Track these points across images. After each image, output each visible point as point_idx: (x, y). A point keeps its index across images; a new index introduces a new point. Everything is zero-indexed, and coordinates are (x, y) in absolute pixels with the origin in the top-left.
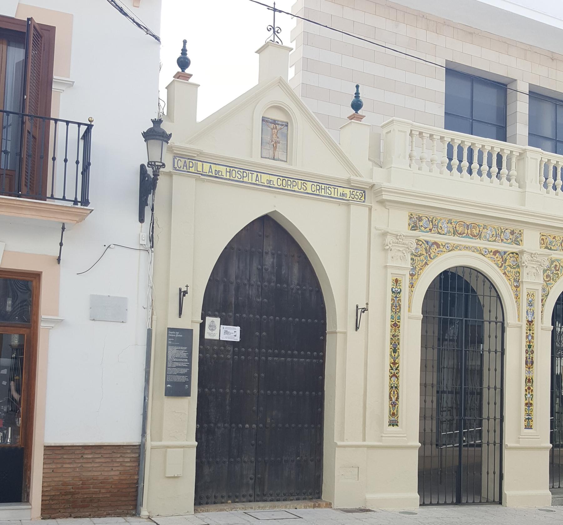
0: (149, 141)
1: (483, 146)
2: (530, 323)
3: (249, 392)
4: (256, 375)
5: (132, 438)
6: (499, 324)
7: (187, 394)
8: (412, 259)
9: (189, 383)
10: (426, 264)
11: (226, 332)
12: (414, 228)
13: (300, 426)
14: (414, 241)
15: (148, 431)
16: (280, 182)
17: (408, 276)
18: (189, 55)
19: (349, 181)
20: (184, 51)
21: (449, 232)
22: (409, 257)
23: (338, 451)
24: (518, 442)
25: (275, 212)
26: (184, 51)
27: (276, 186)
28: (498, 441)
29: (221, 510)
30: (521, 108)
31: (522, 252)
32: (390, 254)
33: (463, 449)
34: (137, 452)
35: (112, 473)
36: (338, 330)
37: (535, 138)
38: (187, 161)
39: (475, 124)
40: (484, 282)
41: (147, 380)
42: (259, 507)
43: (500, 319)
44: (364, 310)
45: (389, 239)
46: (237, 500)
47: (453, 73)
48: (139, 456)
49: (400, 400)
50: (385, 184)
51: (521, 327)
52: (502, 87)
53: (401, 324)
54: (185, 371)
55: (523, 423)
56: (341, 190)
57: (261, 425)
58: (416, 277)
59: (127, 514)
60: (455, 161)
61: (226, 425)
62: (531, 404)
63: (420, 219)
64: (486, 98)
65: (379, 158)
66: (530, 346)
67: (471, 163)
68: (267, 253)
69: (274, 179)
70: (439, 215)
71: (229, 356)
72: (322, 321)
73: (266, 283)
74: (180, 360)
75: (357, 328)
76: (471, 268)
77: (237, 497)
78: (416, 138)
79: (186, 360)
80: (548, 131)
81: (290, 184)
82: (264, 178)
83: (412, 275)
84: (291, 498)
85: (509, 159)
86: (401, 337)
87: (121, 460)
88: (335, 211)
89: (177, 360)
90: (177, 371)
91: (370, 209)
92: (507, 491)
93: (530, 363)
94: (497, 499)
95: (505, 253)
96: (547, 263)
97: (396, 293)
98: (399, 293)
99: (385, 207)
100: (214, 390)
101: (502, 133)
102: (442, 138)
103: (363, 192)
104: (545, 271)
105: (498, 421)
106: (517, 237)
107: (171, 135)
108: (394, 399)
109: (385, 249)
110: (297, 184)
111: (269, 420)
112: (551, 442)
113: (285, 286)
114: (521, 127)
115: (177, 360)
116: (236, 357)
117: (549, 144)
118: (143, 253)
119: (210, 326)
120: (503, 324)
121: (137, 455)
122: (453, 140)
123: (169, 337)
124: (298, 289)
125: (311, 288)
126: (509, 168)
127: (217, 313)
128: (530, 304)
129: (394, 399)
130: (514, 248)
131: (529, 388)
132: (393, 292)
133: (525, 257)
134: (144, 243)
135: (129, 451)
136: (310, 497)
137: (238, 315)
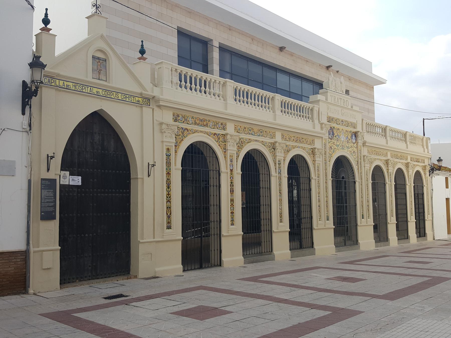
1: (206, 78)
2: (231, 170)
3: (87, 215)
4: (91, 205)
5: (20, 246)
6: (217, 171)
7: (55, 218)
8: (176, 137)
10: (182, 140)
11: (73, 180)
12: (176, 120)
13: (117, 233)
14: (177, 128)
15: (31, 242)
16: (103, 93)
17: (236, 154)
18: (49, 17)
19: (141, 94)
20: (46, 15)
21: (192, 123)
22: (174, 136)
23: (141, 246)
24: (228, 233)
25: (101, 110)
26: (46, 15)
27: (102, 95)
28: (218, 233)
29: (75, 286)
30: (216, 55)
31: (227, 134)
32: (165, 135)
33: (203, 238)
34: (24, 255)
35: (10, 269)
36: (139, 177)
37: (223, 73)
38: (50, 79)
39: (192, 62)
40: (210, 149)
41: (29, 211)
42: (97, 282)
43: (218, 169)
44: (153, 165)
45: (164, 126)
46: (82, 280)
47: (182, 34)
48: (26, 257)
49: (172, 214)
50: (161, 97)
51: (227, 173)
52: (205, 43)
53: (171, 173)
54: (52, 204)
55: (230, 223)
56: (137, 98)
57: (95, 234)
58: (177, 147)
59: (20, 293)
60: (183, 83)
61: (74, 235)
62: (233, 212)
63: (178, 116)
64: (197, 48)
65: (156, 83)
66: (232, 183)
67: (191, 84)
68: (95, 133)
69: (100, 91)
70: (187, 114)
71: (75, 194)
72: (128, 172)
73: (95, 151)
74: (49, 198)
75: (149, 176)
76: (200, 142)
77: (81, 278)
78: (173, 72)
79: (53, 198)
80: (228, 69)
81: (108, 94)
83: (176, 146)
84: (113, 275)
85: (210, 83)
86: (171, 180)
87: (15, 260)
88: (134, 110)
89: (47, 198)
90: (47, 204)
91: (153, 110)
92: (224, 259)
93: (232, 191)
94: (219, 264)
95: (219, 134)
96: (238, 140)
97: (168, 156)
98: (170, 156)
99: (160, 109)
100: (66, 215)
101: (206, 70)
102: (176, 70)
103: (148, 101)
104: (237, 144)
105: (218, 222)
106: (224, 127)
108: (169, 214)
109: (162, 132)
111: (99, 231)
112: (243, 232)
113: (107, 152)
114: (216, 67)
115: (47, 198)
116: (79, 194)
117: (228, 75)
118: (25, 134)
119: (63, 176)
120: (219, 171)
121: (24, 257)
122: (192, 74)
124: (114, 154)
125: (121, 153)
126: (210, 88)
127: (67, 169)
128: (231, 161)
129: (169, 214)
130: (223, 132)
131: (232, 204)
132: (167, 155)
133: (228, 137)
134: (26, 127)
135: (19, 255)
136: (124, 273)
137: (80, 169)
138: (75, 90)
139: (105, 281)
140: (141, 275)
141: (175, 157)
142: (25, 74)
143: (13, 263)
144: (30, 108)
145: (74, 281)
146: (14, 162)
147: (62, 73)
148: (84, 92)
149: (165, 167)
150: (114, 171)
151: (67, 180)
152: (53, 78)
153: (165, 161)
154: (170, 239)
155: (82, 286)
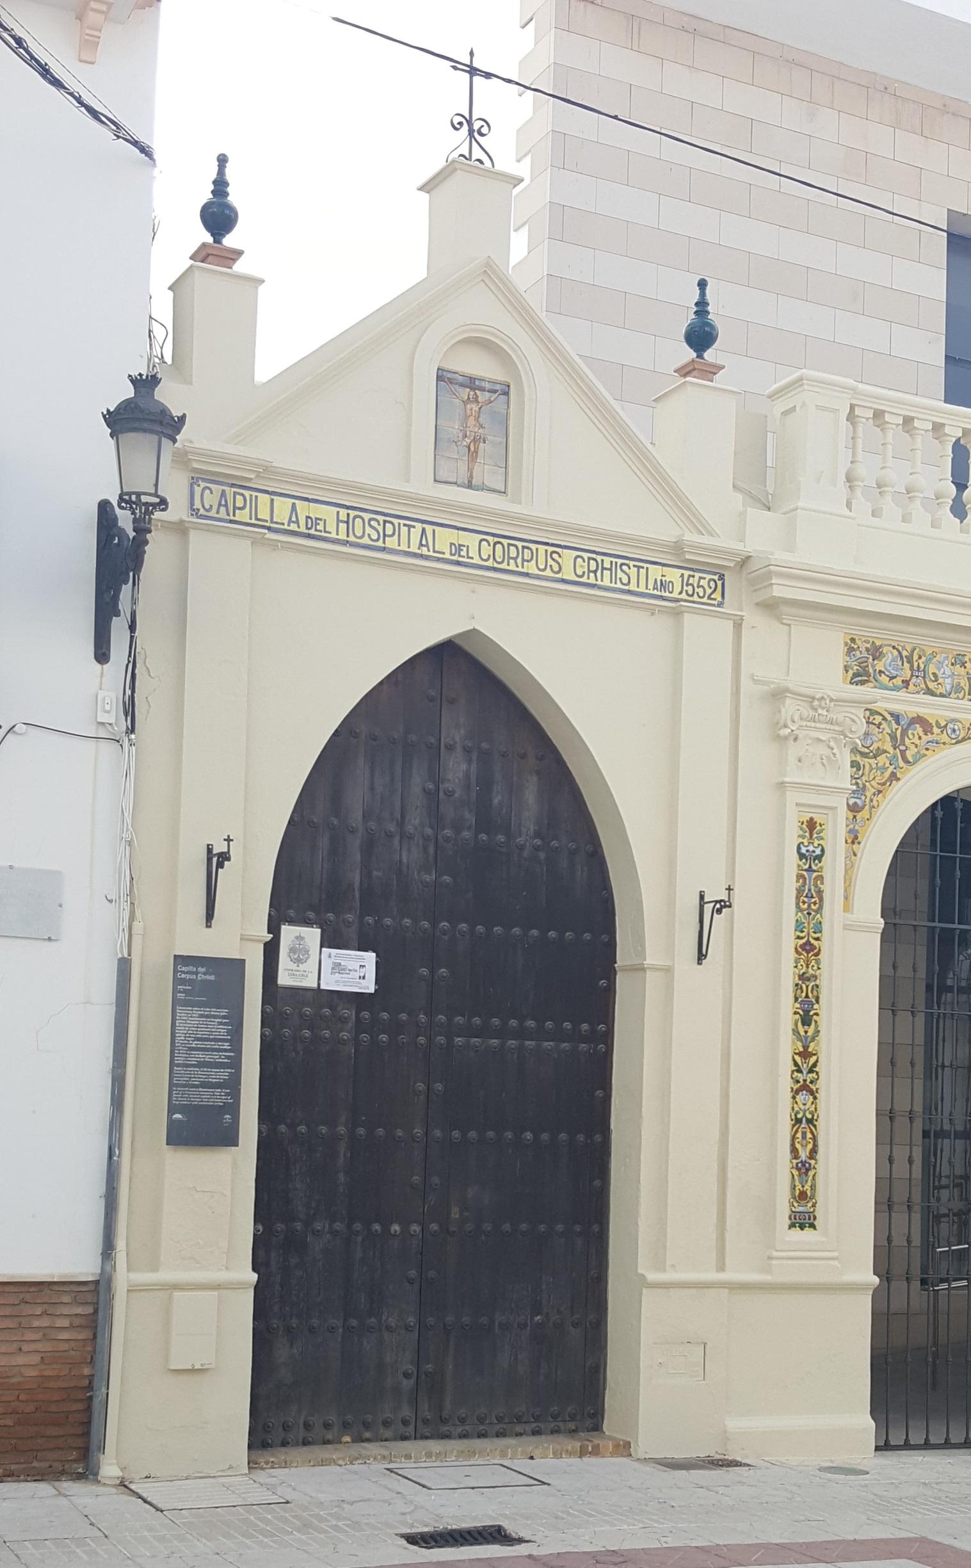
0: (127, 438)
3: (399, 1133)
4: (421, 1086)
8: (854, 764)
9: (233, 1108)
10: (894, 777)
11: (337, 968)
12: (860, 677)
15: (121, 1244)
16: (486, 550)
17: (843, 812)
18: (234, 197)
19: (678, 547)
20: (220, 186)
22: (847, 758)
23: (649, 1299)
26: (220, 186)
29: (323, 1463)
32: (793, 751)
34: (91, 1299)
35: (21, 1360)
36: (649, 961)
38: (230, 491)
42: (429, 1455)
44: (722, 906)
45: (791, 708)
46: (367, 1435)
48: (96, 1311)
49: (820, 1155)
50: (780, 556)
53: (824, 945)
54: (223, 1075)
56: (655, 572)
57: (434, 1227)
58: (865, 813)
59: (63, 1472)
61: (338, 1226)
63: (876, 652)
68: (450, 748)
69: (472, 540)
71: (345, 1035)
73: (448, 832)
74: (209, 1044)
77: (367, 1426)
78: (865, 425)
79: (226, 1046)
82: (444, 540)
83: (854, 809)
84: (519, 1428)
86: (823, 982)
87: (45, 1322)
88: (636, 632)
90: (200, 1075)
91: (738, 626)
97: (811, 859)
98: (819, 858)
100: (302, 1129)
102: (878, 415)
103: (719, 578)
107: (183, 419)
108: (803, 1155)
109: (780, 737)
110: (534, 556)
111: (455, 1213)
113: (501, 838)
116: (364, 1037)
118: (107, 748)
119: (292, 950)
121: (89, 1310)
123: (177, 981)
124: (537, 848)
127: (311, 915)
129: (803, 1155)
132: (802, 856)
136: (572, 1425)
137: (370, 920)
138: (345, 543)
139: (472, 1454)
140: (644, 1446)
141: (849, 869)
142: (94, 469)
143: (38, 1336)
144: (132, 627)
145: (330, 1437)
146: (56, 875)
147: (281, 461)
148: (392, 551)
149: (790, 914)
150: (535, 932)
151: (311, 965)
152: (241, 485)
153: (791, 886)
154: (803, 1278)
155: (356, 1467)
